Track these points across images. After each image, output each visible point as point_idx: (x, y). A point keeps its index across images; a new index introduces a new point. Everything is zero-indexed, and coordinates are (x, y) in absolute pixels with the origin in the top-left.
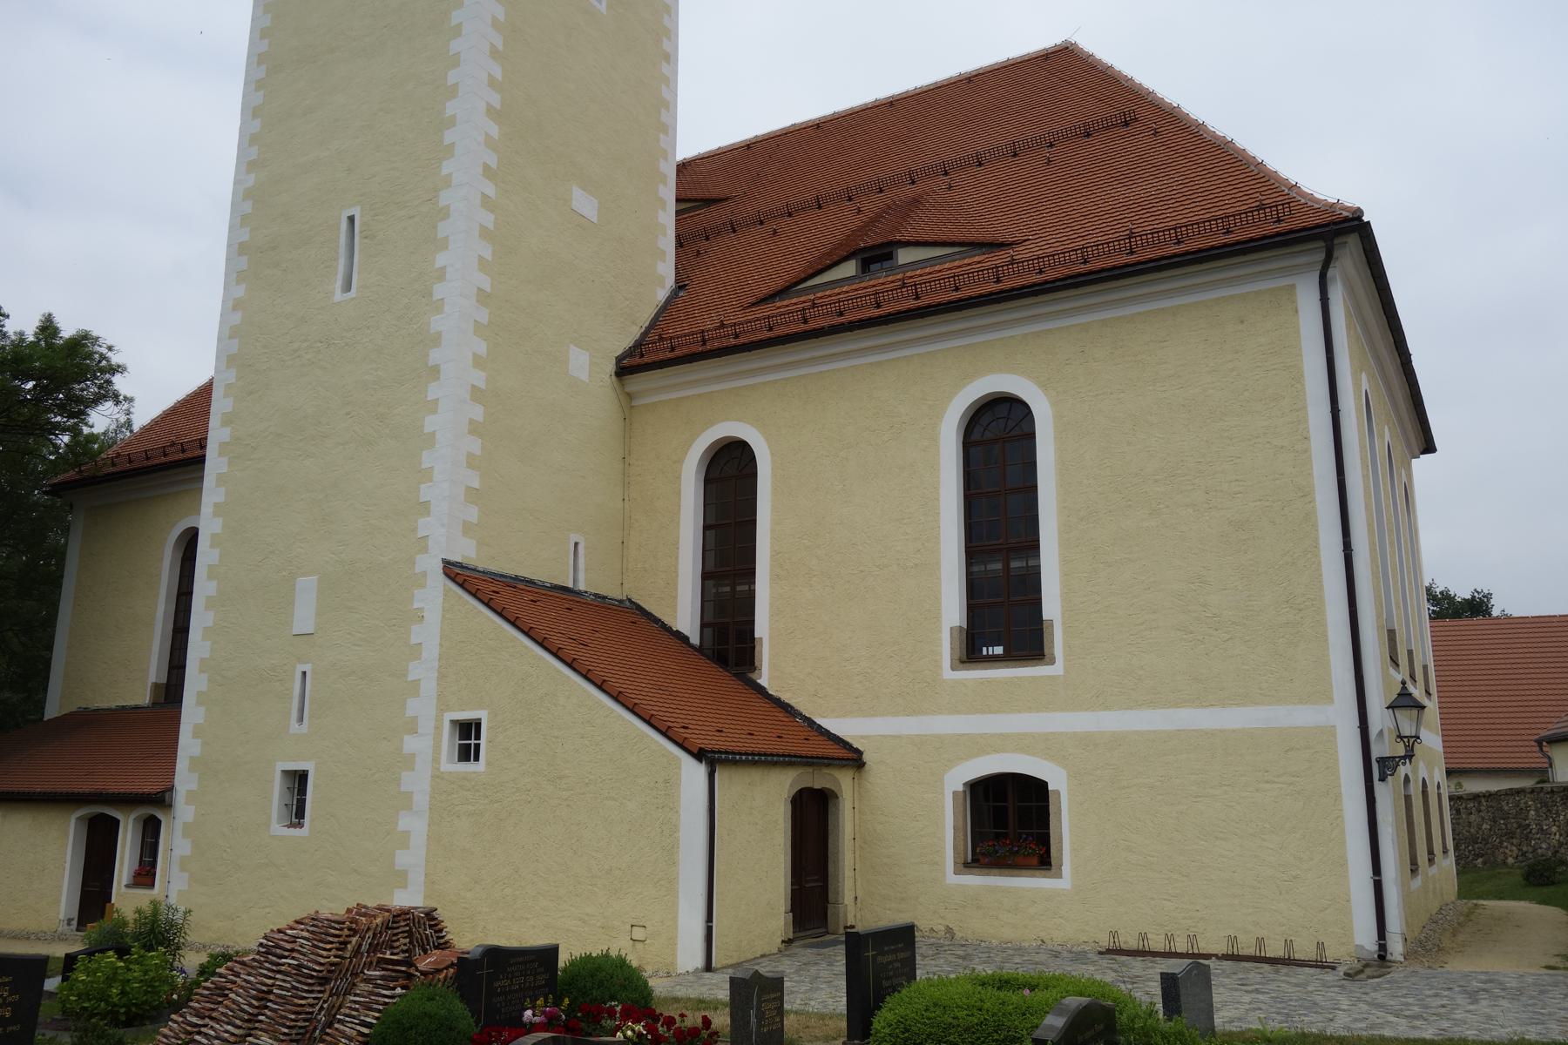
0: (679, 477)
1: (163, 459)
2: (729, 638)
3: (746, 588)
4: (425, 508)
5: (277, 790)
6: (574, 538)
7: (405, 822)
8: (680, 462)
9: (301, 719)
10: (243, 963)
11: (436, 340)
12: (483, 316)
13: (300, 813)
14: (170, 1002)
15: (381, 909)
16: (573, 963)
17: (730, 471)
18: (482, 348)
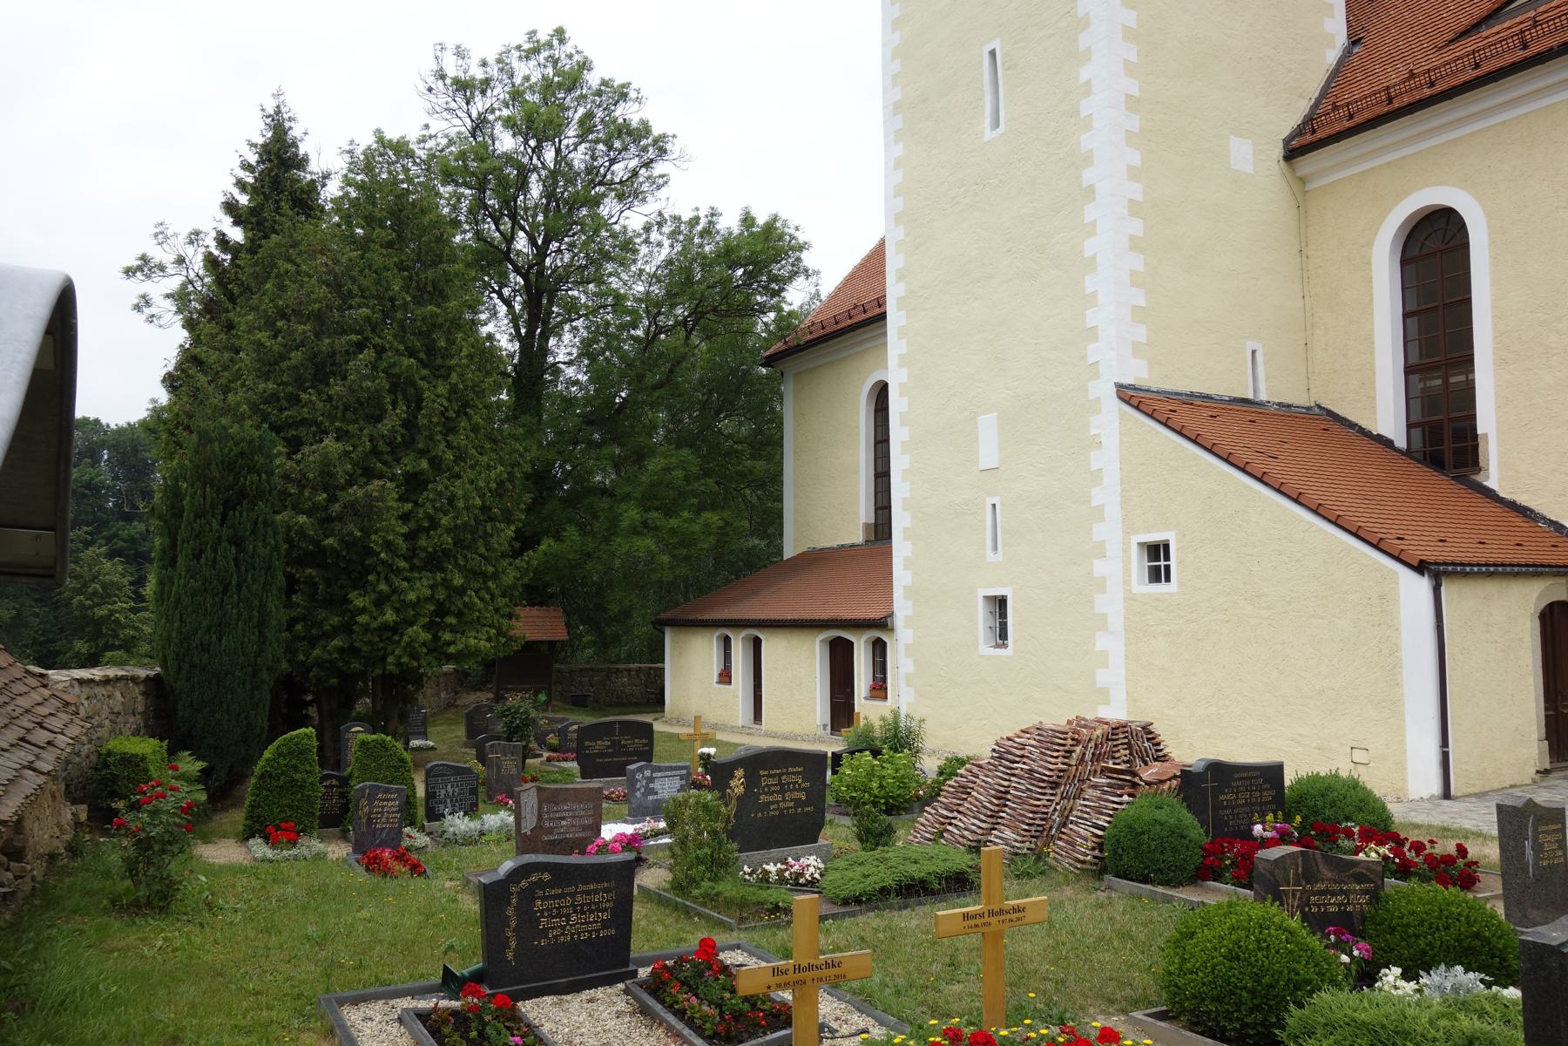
0: (1369, 263)
1: (849, 322)
2: (1445, 437)
3: (1463, 378)
4: (1092, 334)
5: (981, 616)
6: (1251, 345)
7: (1102, 642)
8: (1370, 244)
9: (995, 548)
10: (980, 766)
11: (1088, 159)
12: (1134, 123)
13: (1003, 635)
14: (918, 798)
15: (1101, 721)
16: (1299, 781)
17: (1435, 249)
18: (1136, 158)
